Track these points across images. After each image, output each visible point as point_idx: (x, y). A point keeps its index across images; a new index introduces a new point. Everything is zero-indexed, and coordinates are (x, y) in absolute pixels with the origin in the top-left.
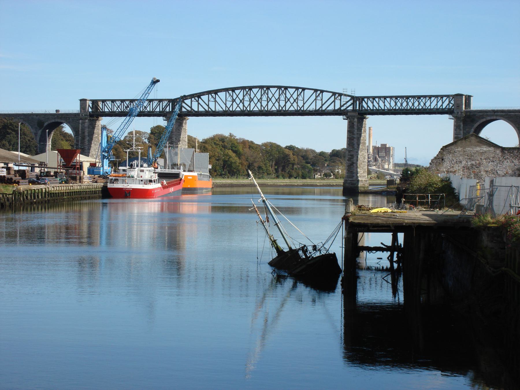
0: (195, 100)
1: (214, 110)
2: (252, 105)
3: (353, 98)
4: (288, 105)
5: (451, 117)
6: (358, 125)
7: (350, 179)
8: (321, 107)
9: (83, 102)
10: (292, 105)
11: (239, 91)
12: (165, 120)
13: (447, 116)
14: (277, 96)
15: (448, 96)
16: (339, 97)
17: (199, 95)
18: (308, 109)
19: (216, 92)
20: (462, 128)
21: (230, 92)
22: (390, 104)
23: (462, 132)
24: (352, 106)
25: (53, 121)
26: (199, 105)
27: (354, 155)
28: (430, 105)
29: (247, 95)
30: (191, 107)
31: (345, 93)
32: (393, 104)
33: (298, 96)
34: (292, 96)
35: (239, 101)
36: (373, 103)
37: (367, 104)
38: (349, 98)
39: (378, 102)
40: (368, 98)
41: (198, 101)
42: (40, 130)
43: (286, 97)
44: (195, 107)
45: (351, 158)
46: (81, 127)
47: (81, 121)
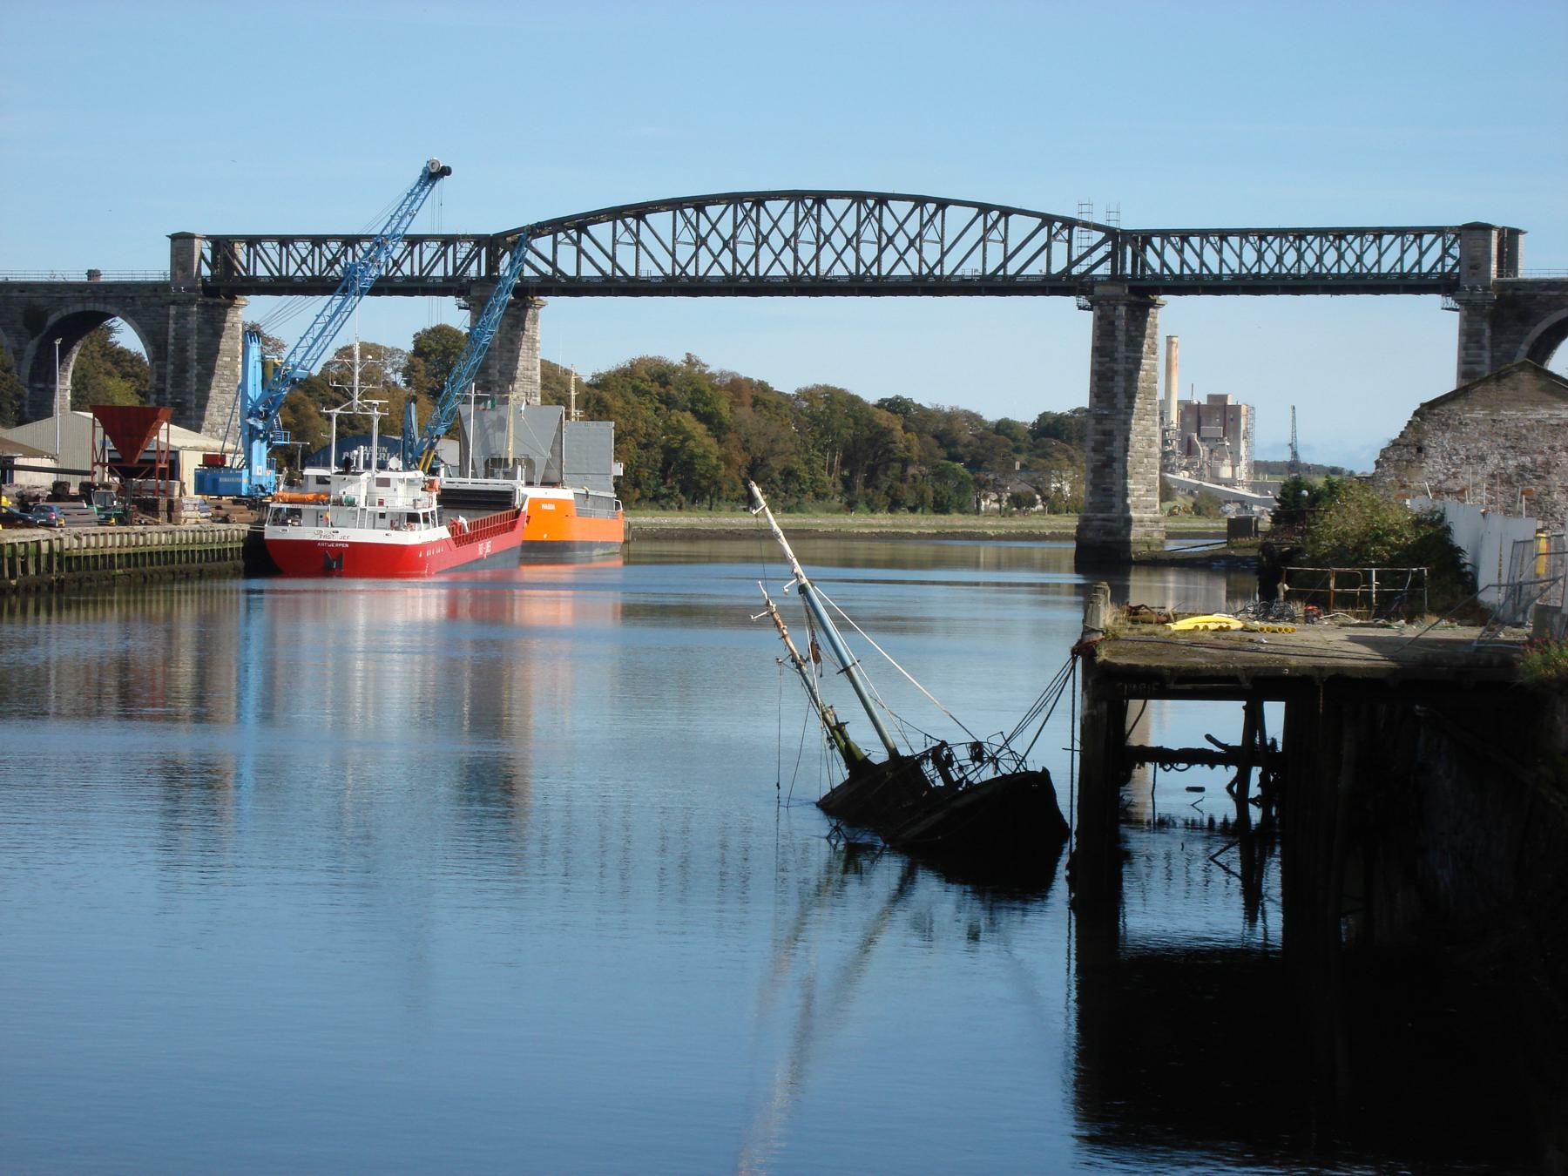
0: (567, 240)
1: (632, 273)
2: (766, 256)
3: (1111, 234)
4: (827, 256)
5: (1451, 302)
6: (1128, 330)
7: (1101, 515)
8: (1003, 266)
9: (182, 242)
10: (901, 257)
11: (784, 203)
12: (465, 308)
13: (1435, 300)
14: (849, 225)
15: (1439, 231)
16: (1065, 233)
17: (581, 223)
18: (958, 273)
19: (640, 211)
20: (1486, 341)
21: (689, 212)
22: (1238, 258)
23: (1486, 355)
24: (1108, 264)
25: (79, 308)
26: (583, 258)
27: (1115, 433)
28: (1378, 262)
29: (747, 223)
30: (553, 264)
31: (1085, 218)
32: (1250, 256)
33: (923, 226)
34: (901, 226)
35: (771, 240)
36: (1180, 252)
37: (1160, 255)
38: (1099, 236)
39: (1198, 250)
40: (1165, 234)
41: (577, 243)
42: (33, 338)
43: (881, 229)
44: (567, 265)
45: (1103, 444)
46: (175, 330)
47: (173, 310)
